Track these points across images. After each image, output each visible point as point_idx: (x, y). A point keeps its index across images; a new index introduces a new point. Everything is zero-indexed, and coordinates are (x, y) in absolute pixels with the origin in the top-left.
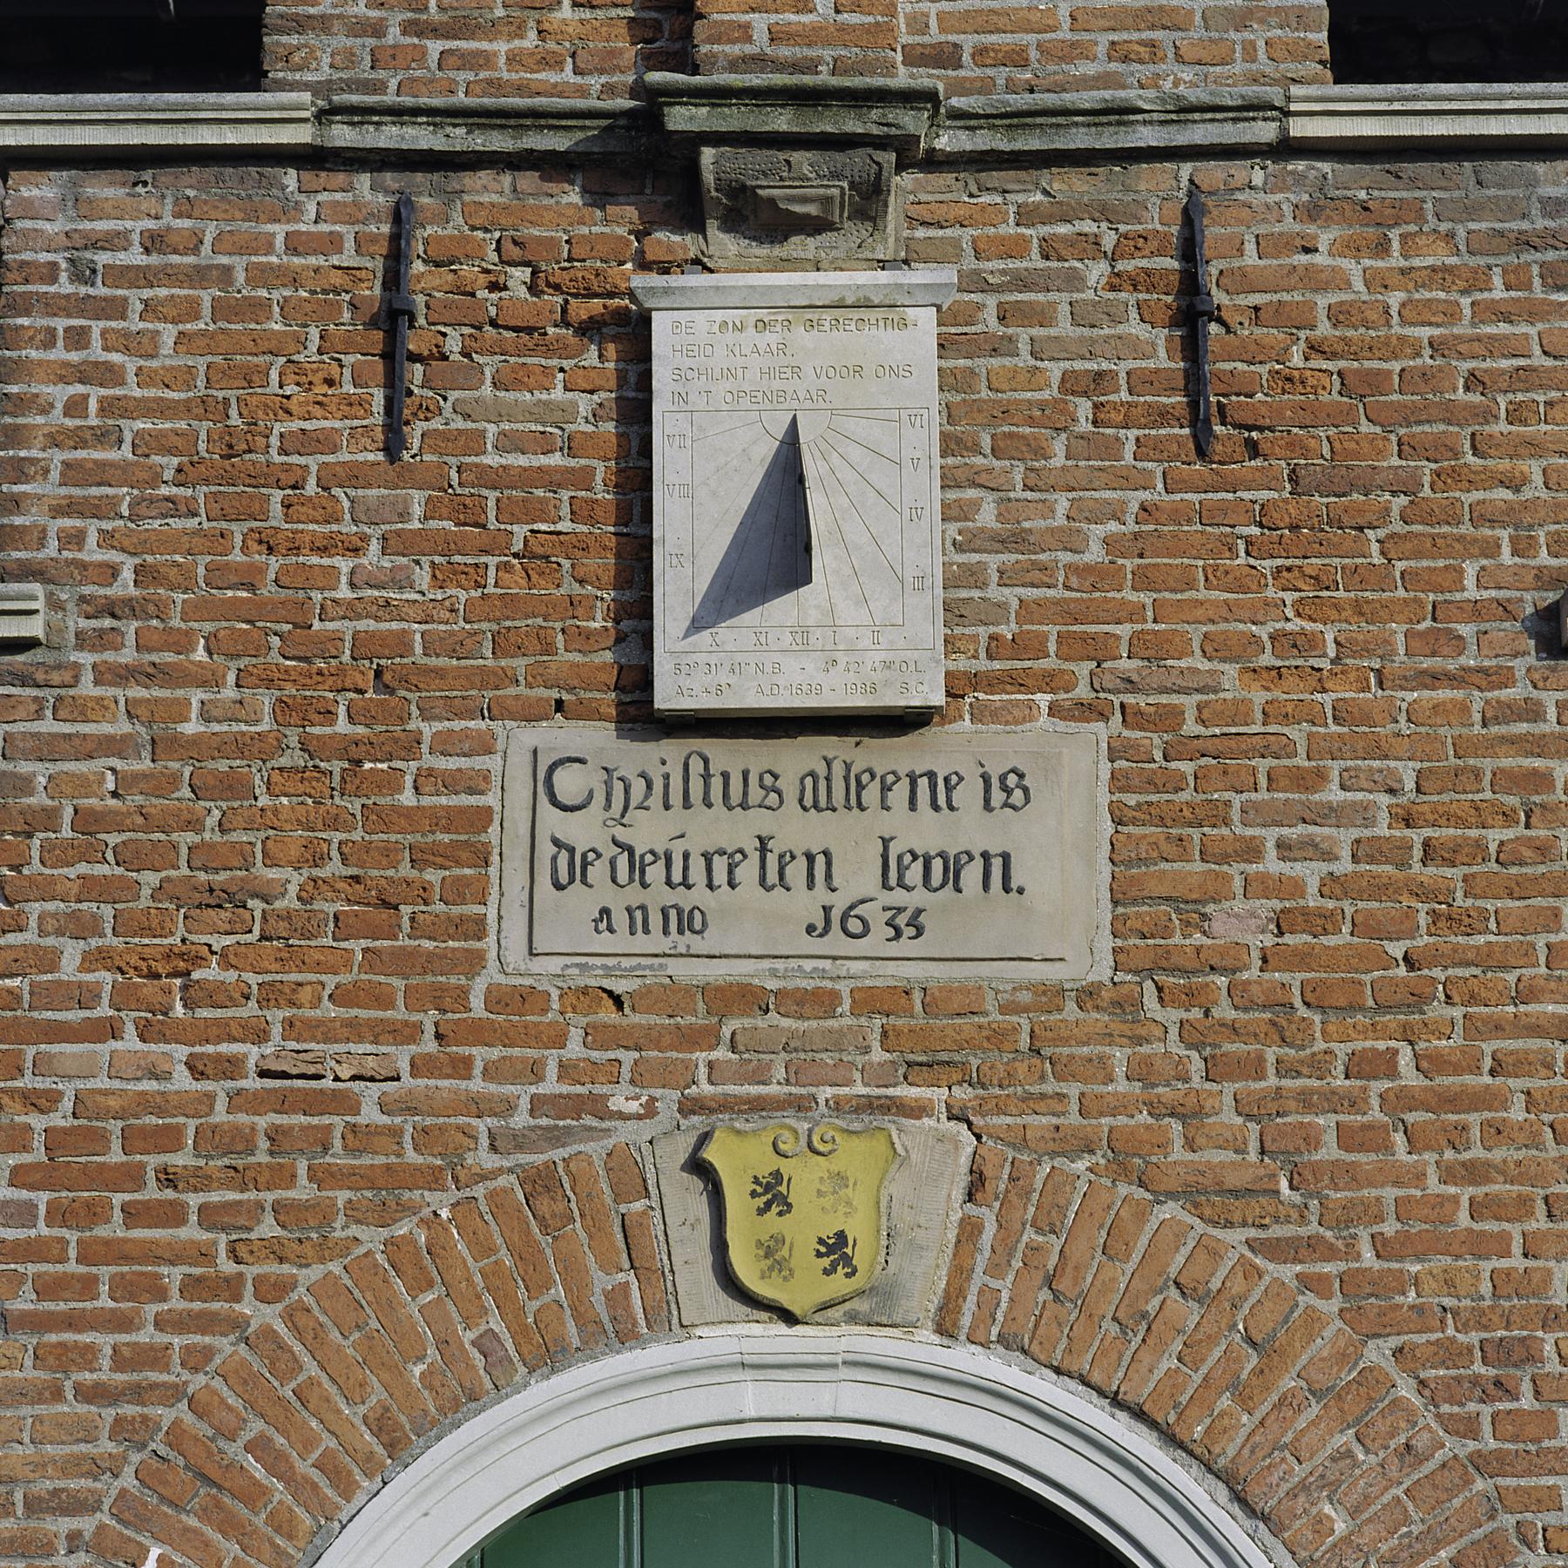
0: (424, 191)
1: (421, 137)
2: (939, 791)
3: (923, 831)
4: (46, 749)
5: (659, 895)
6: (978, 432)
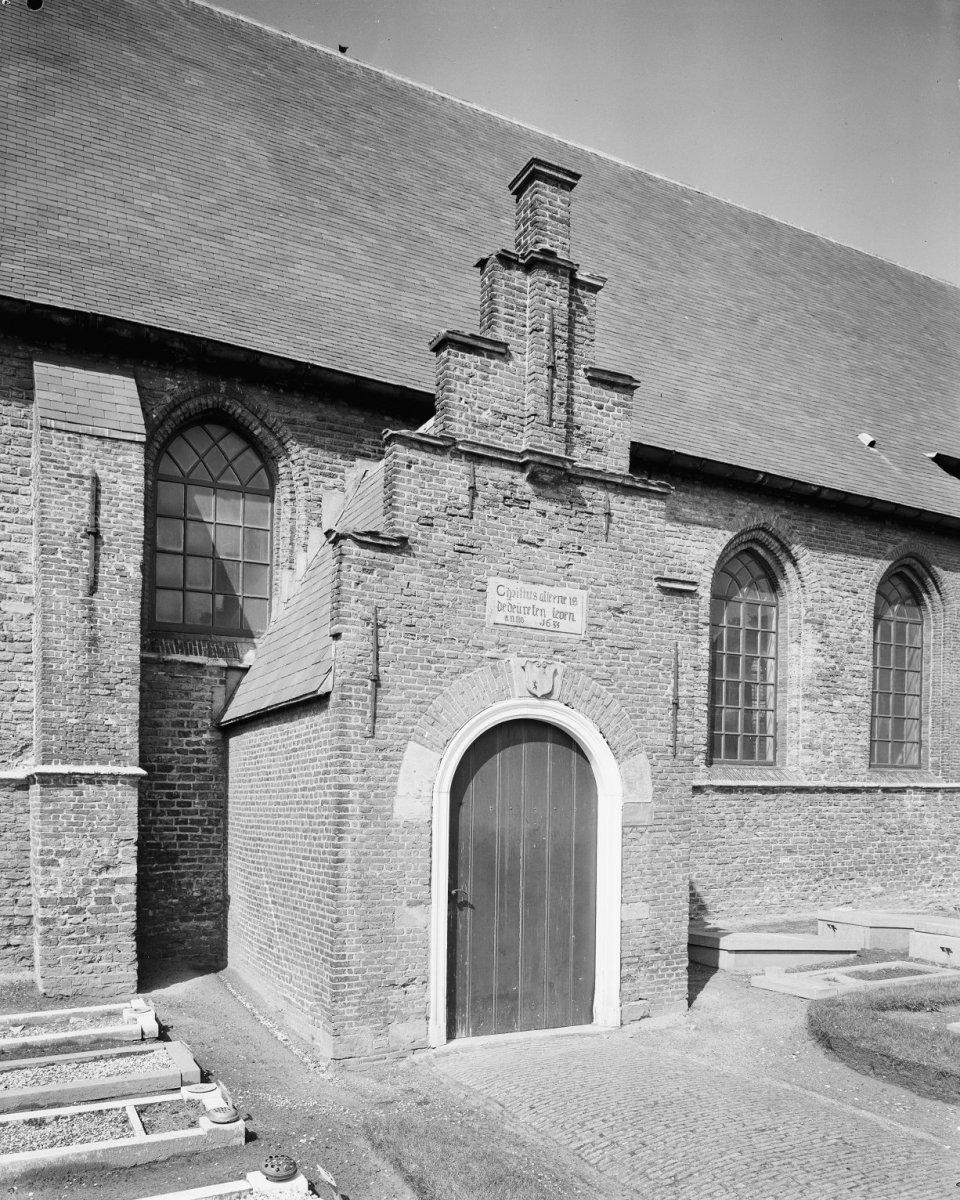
3: (560, 607)
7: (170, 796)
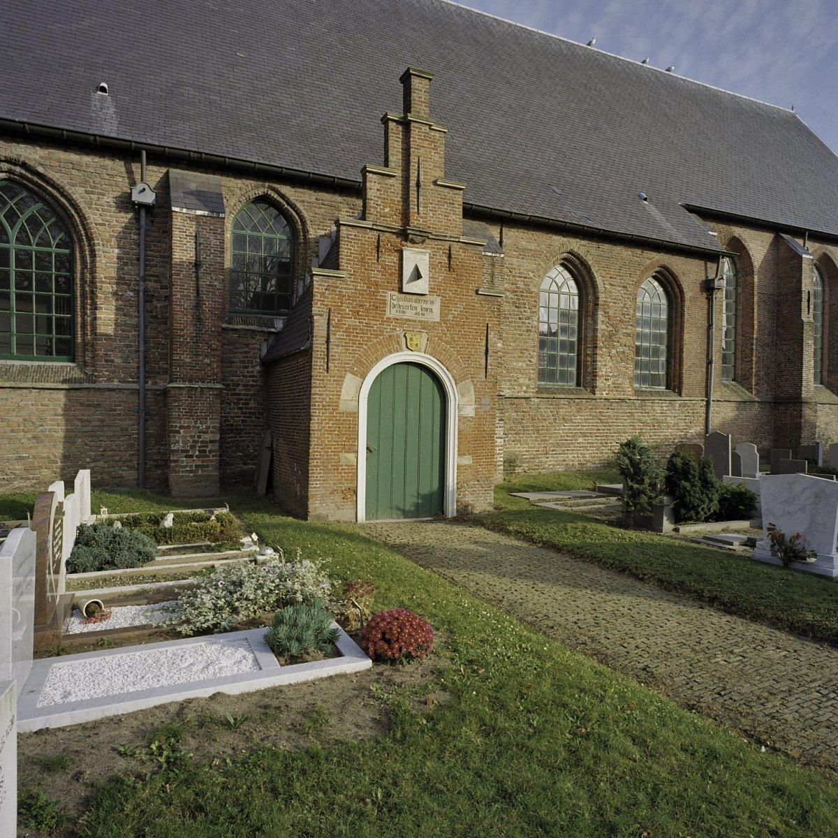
0: (381, 234)
1: (382, 229)
2: (426, 302)
3: (425, 306)
4: (345, 288)
5: (402, 309)
6: (432, 266)
7: (238, 399)
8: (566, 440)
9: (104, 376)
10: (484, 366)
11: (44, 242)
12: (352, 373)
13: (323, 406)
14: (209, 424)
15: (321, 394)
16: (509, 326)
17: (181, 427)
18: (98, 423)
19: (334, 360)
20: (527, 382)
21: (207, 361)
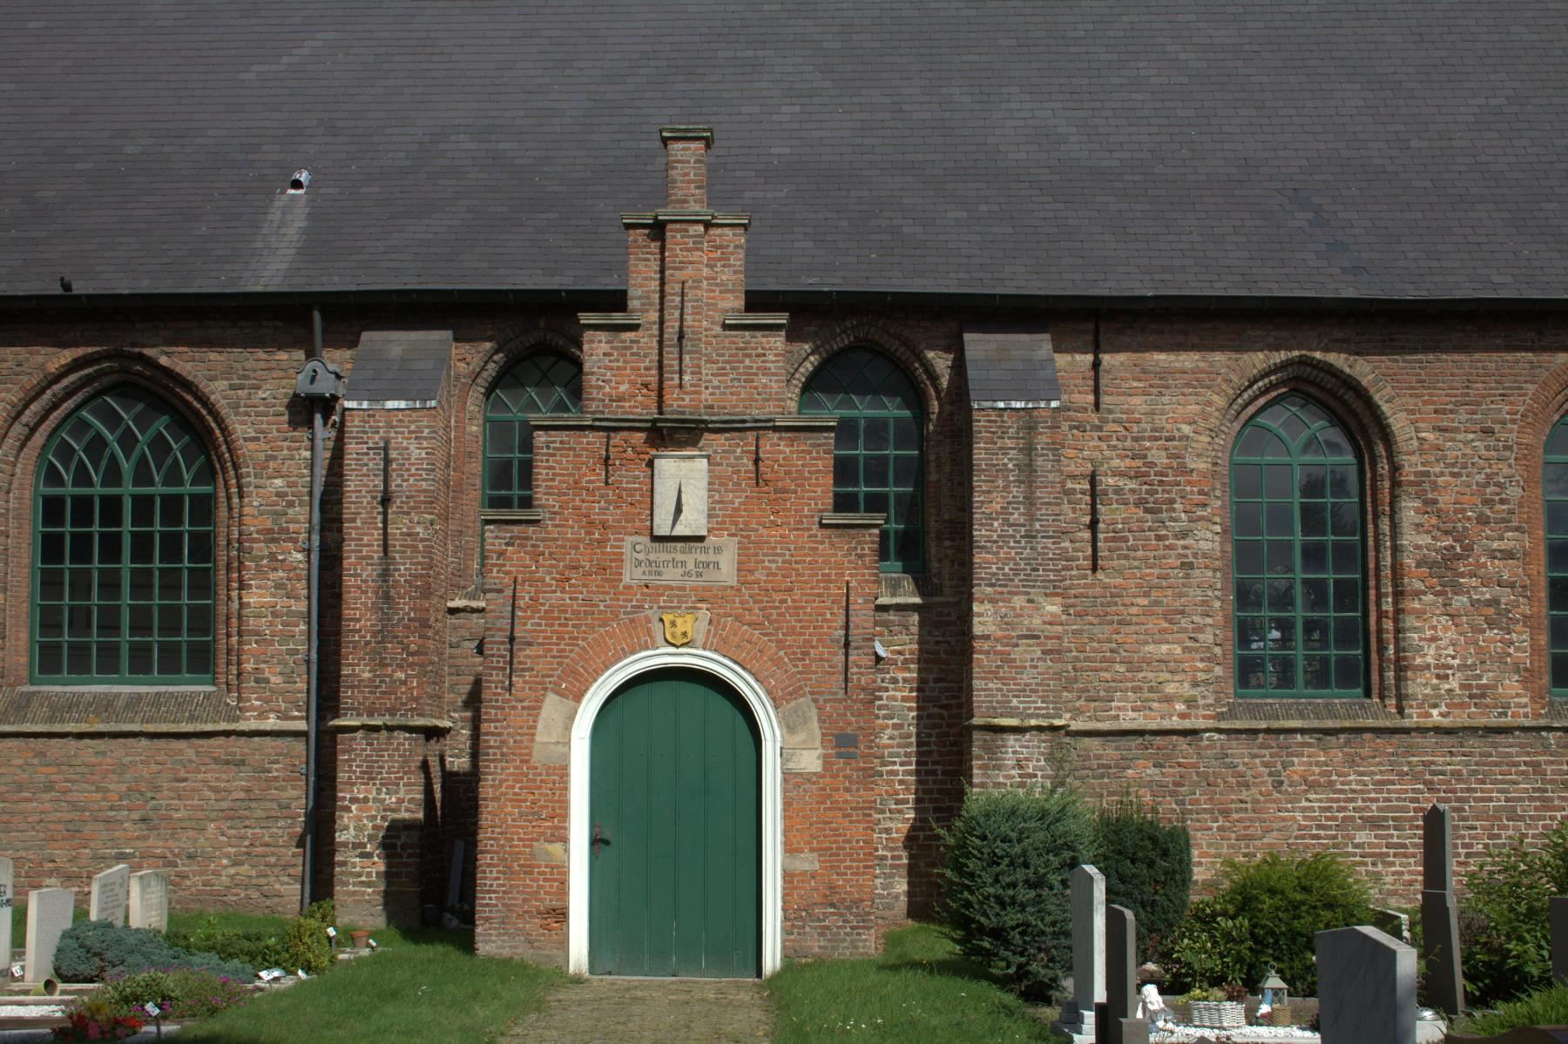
2: (706, 551)
3: (702, 557)
6: (715, 483)
8: (1317, 837)
9: (253, 709)
10: (841, 667)
11: (173, 477)
12: (558, 693)
13: (503, 754)
14: (401, 795)
15: (499, 734)
16: (1126, 557)
17: (354, 800)
18: (242, 795)
19: (523, 670)
20: (1186, 690)
21: (401, 675)
